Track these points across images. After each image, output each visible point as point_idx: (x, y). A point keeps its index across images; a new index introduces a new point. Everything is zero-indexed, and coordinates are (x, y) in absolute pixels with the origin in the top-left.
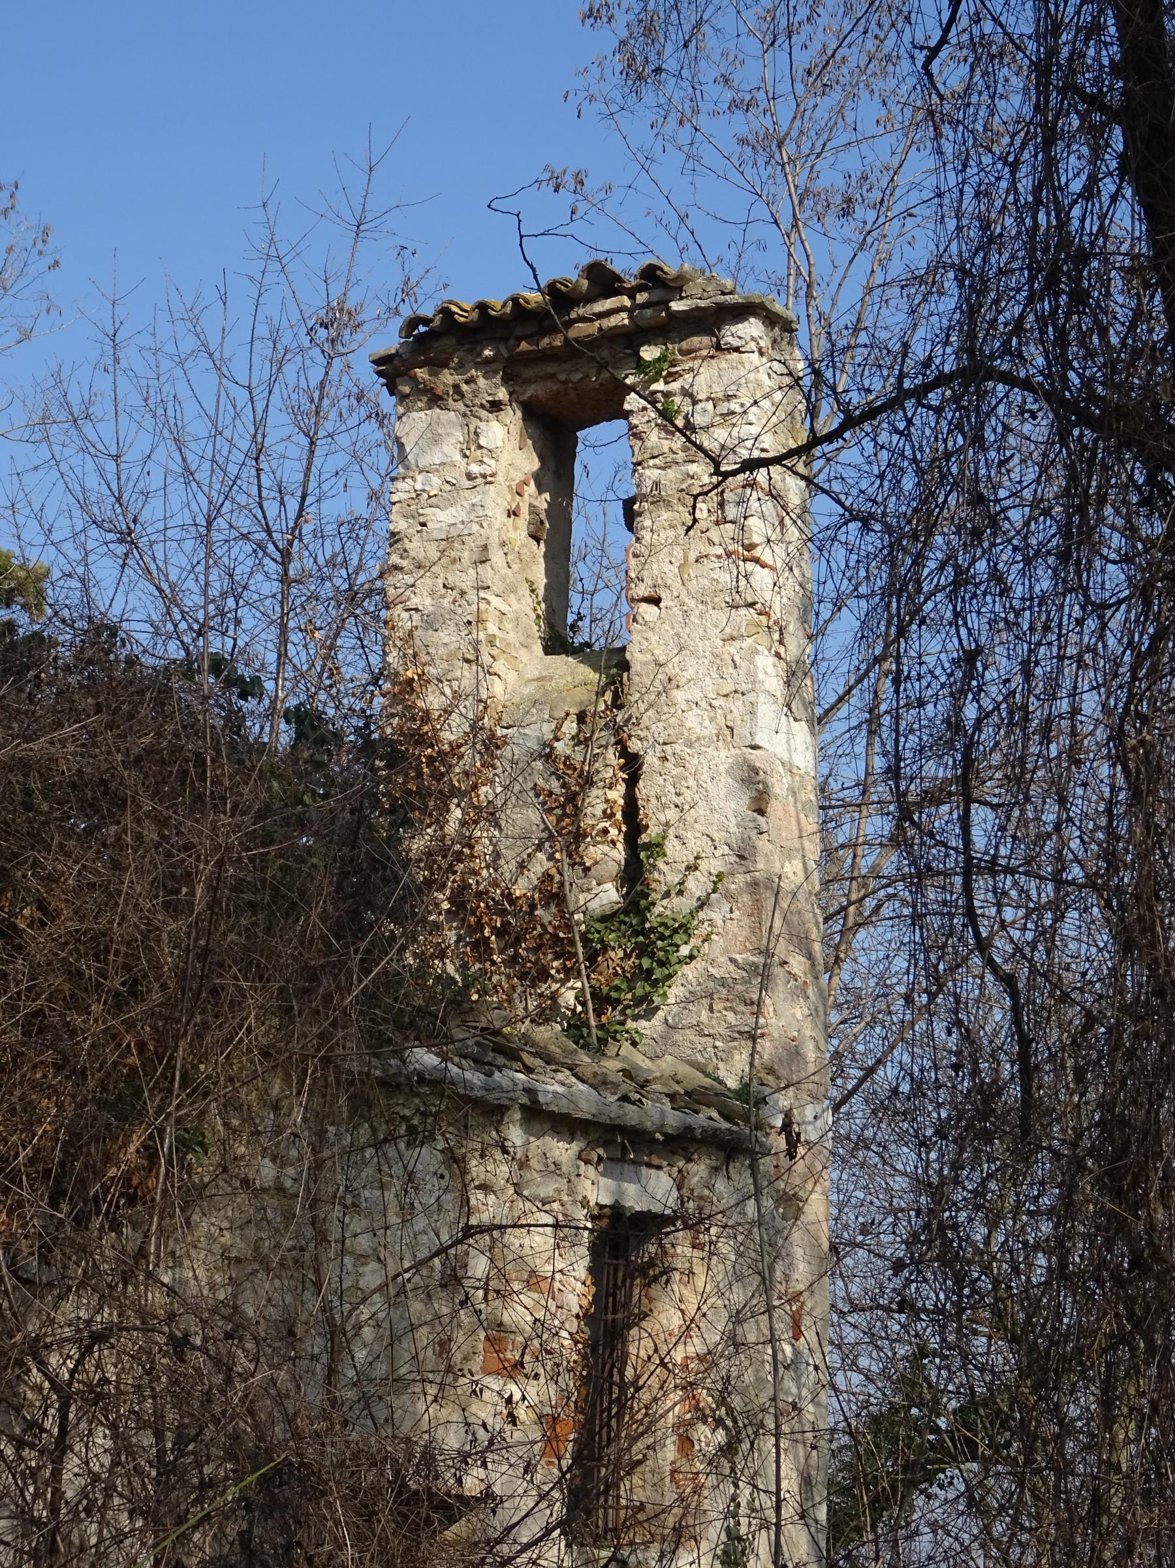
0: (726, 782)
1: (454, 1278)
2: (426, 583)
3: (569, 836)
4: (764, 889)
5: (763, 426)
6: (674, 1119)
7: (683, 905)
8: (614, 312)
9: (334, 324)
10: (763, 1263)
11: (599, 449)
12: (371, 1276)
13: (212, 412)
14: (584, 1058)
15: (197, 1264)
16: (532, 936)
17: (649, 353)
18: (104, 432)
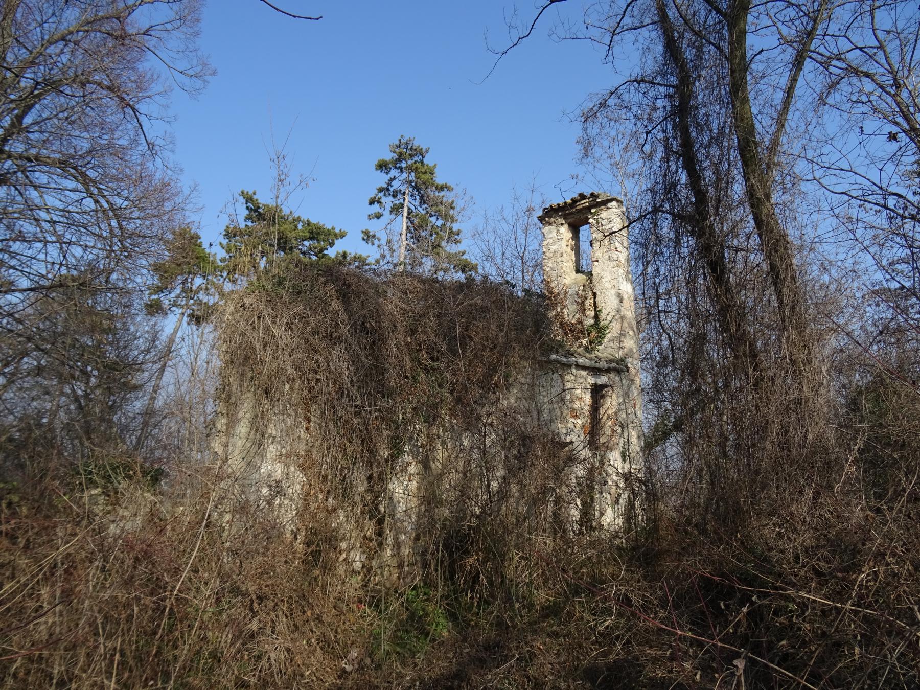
0: (614, 297)
1: (563, 400)
2: (550, 261)
3: (583, 311)
4: (623, 318)
5: (617, 224)
6: (606, 366)
7: (607, 322)
8: (585, 203)
9: (530, 210)
10: (626, 395)
11: (584, 230)
12: (546, 400)
13: (866, 50)
14: (587, 355)
15: (511, 400)
16: (576, 331)
17: (593, 211)
18: (485, 236)
